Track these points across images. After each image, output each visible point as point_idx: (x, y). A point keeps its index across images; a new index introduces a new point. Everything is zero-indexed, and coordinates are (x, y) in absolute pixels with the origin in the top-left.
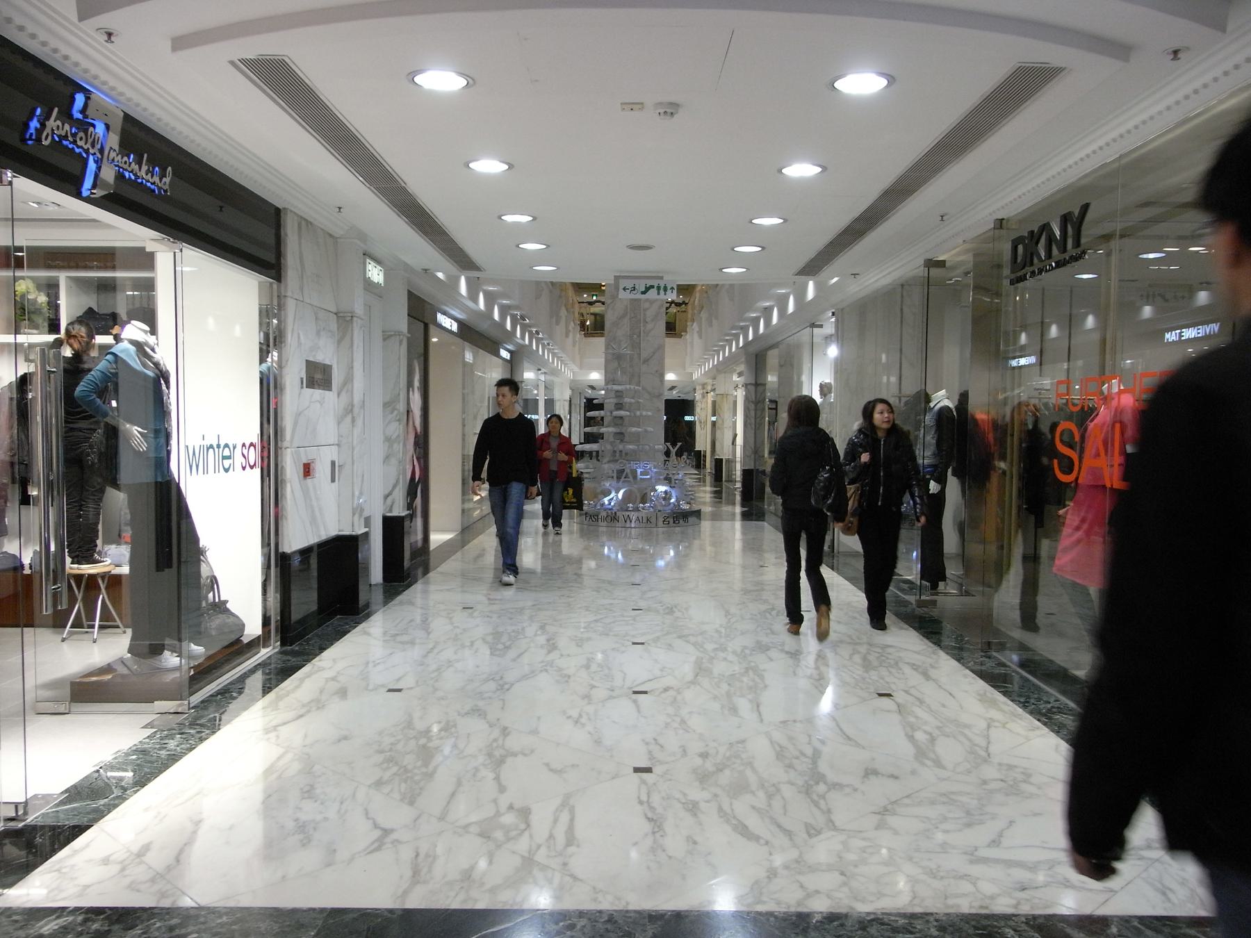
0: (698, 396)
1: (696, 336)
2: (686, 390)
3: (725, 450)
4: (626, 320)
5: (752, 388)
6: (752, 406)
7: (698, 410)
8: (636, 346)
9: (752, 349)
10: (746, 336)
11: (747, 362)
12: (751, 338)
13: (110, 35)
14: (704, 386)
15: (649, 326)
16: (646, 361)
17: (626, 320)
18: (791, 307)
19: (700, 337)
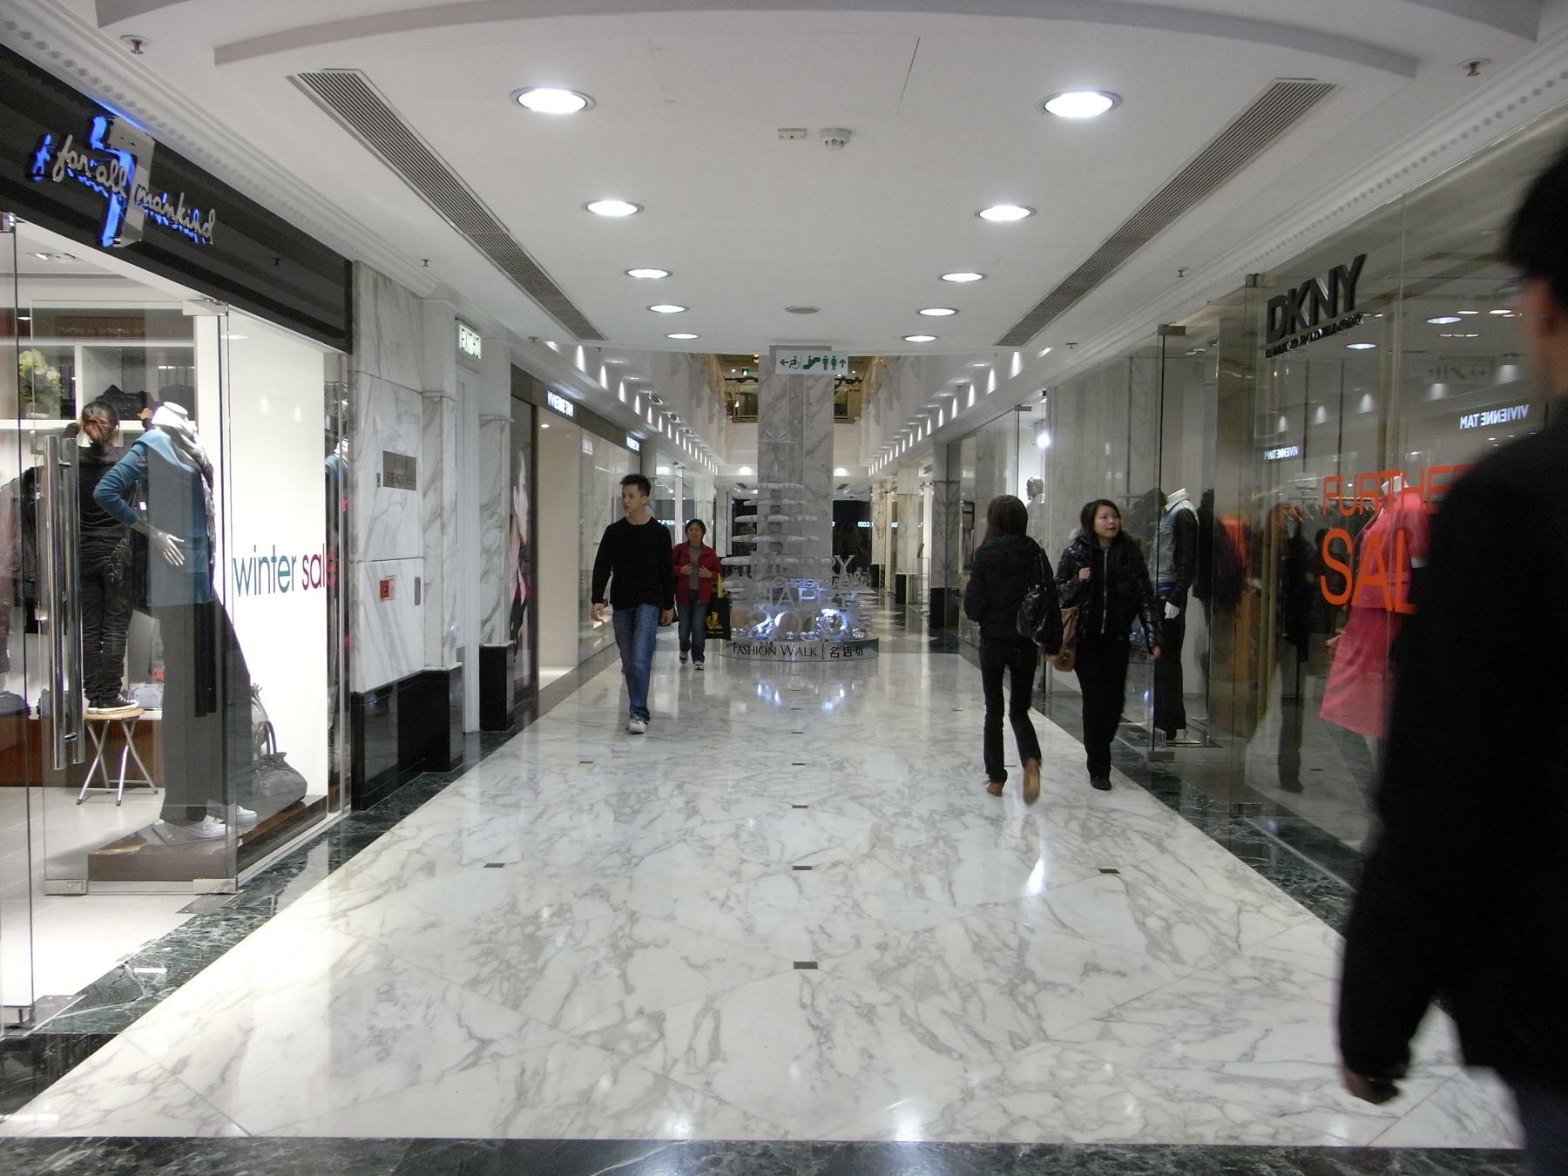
0: (875, 497)
1: (872, 421)
2: (860, 489)
3: (909, 565)
4: (785, 401)
5: (943, 487)
6: (943, 510)
7: (875, 514)
8: (797, 433)
9: (942, 438)
10: (935, 422)
11: (937, 454)
12: (941, 423)
13: (137, 43)
14: (882, 483)
15: (814, 409)
16: (810, 453)
17: (785, 401)
18: (991, 385)
19: (878, 422)
